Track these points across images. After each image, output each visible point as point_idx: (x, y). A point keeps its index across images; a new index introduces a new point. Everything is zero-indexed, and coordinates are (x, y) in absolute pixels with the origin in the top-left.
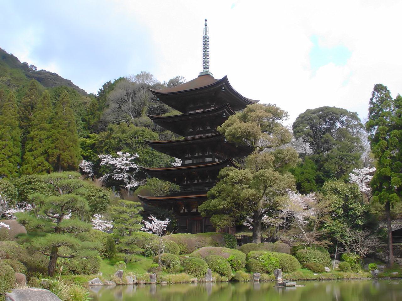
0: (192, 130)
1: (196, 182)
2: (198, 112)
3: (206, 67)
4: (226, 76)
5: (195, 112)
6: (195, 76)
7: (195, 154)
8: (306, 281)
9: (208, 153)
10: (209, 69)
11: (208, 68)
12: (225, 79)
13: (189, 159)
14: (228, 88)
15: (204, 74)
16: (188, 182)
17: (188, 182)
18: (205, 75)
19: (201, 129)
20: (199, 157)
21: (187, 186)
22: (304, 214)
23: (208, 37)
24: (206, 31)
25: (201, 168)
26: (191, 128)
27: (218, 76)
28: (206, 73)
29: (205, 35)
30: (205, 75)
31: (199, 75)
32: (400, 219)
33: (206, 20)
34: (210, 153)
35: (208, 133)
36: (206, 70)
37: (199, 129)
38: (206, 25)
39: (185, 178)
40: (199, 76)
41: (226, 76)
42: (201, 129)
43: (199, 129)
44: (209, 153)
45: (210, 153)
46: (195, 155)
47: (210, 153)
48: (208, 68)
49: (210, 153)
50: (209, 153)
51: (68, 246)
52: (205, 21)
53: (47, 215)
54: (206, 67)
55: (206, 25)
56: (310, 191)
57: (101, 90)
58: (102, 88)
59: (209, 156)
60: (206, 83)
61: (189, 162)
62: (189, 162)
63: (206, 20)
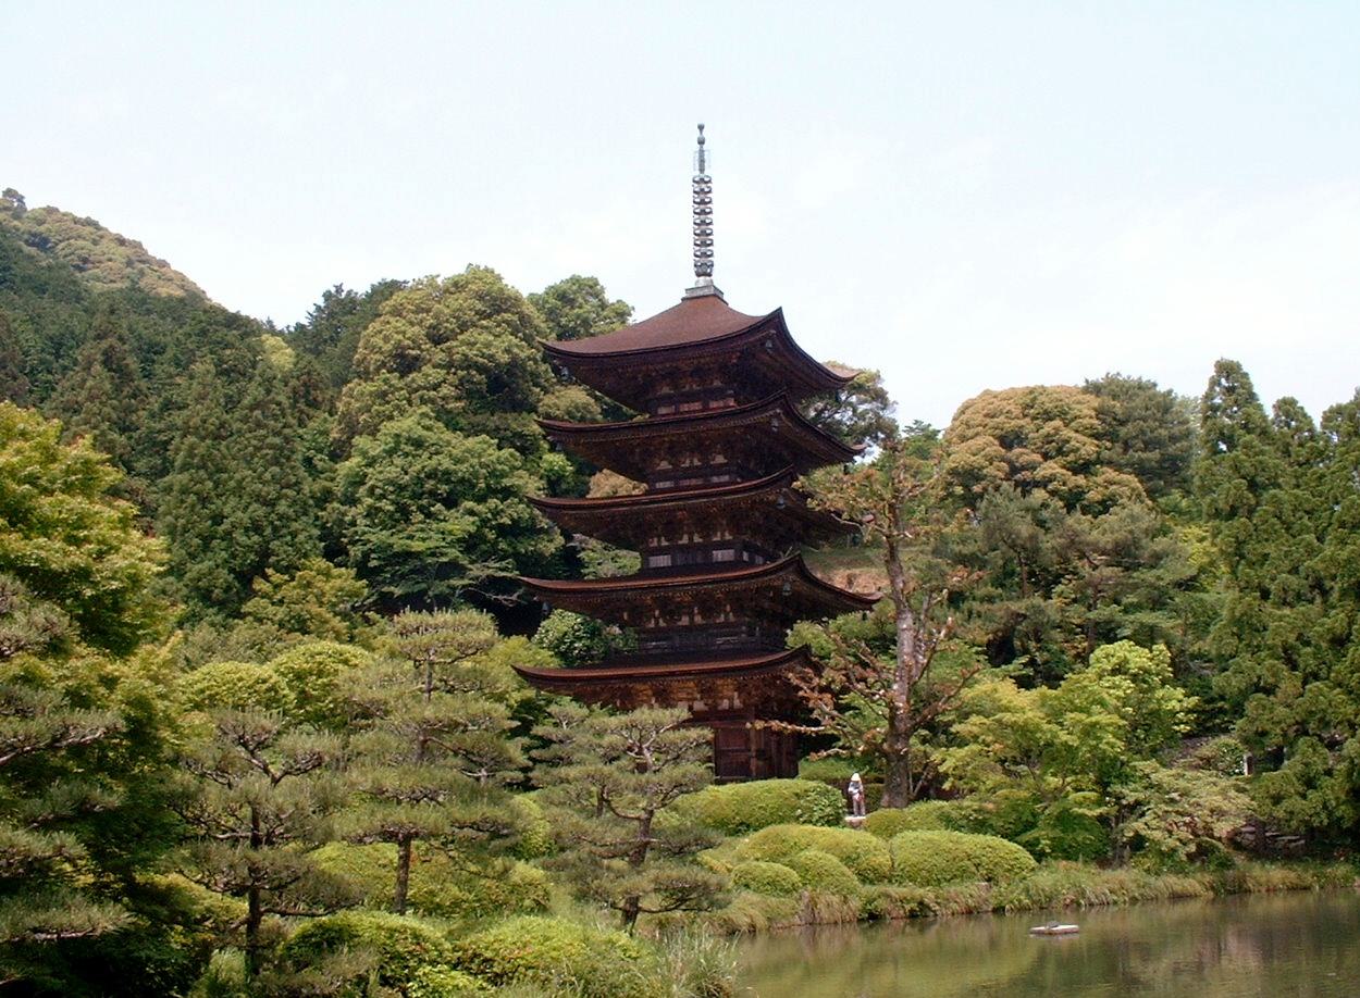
0: (670, 463)
1: (685, 621)
3: (704, 269)
4: (780, 309)
6: (672, 298)
11: (710, 275)
12: (776, 320)
13: (660, 551)
14: (785, 345)
15: (700, 293)
18: (705, 300)
19: (696, 462)
20: (691, 547)
21: (657, 634)
22: (125, 669)
24: (702, 161)
27: (748, 300)
29: (698, 173)
30: (705, 300)
31: (684, 295)
33: (701, 128)
34: (727, 534)
35: (718, 475)
37: (692, 462)
38: (701, 142)
40: (683, 299)
41: (780, 309)
42: (696, 462)
43: (692, 462)
44: (723, 535)
45: (728, 537)
47: (727, 534)
48: (710, 275)
49: (728, 537)
50: (723, 535)
54: (704, 269)
55: (701, 142)
56: (317, 334)
57: (318, 308)
58: (323, 299)
59: (723, 545)
60: (706, 328)
61: (663, 561)
62: (663, 561)
63: (701, 128)
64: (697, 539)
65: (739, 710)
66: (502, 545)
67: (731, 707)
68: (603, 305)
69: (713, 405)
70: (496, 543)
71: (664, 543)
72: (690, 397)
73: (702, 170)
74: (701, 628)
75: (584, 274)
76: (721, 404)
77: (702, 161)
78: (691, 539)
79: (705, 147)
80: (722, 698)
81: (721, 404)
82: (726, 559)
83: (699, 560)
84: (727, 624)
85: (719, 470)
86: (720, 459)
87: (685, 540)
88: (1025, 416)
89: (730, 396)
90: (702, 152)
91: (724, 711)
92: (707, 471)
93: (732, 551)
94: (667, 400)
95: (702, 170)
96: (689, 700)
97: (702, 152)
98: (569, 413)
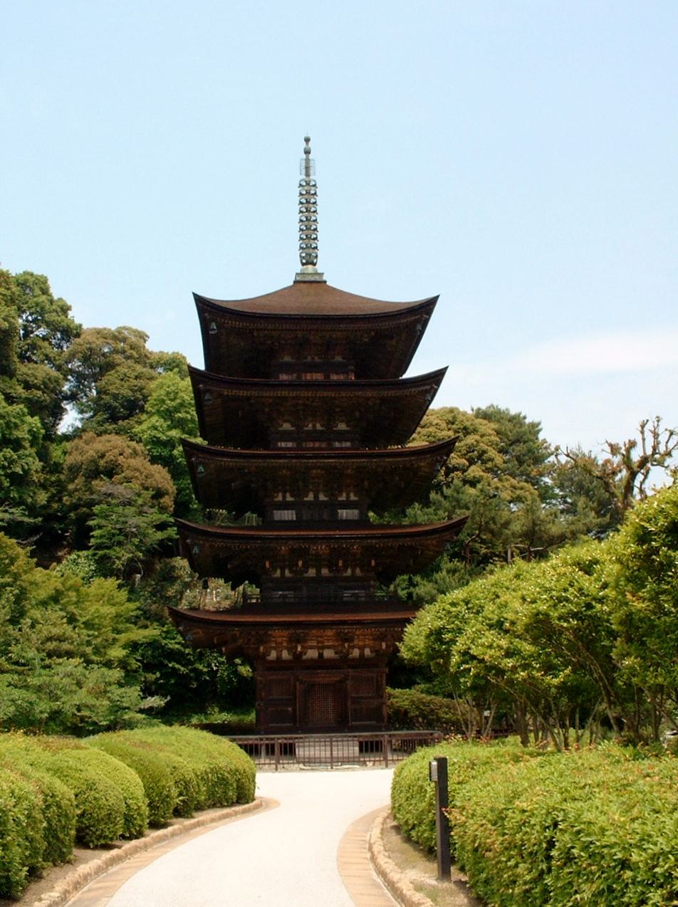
2: (308, 378)
5: (299, 377)
7: (307, 496)
8: (369, 855)
9: (344, 495)
10: (317, 267)
11: (314, 264)
13: (285, 506)
16: (287, 572)
17: (287, 572)
18: (310, 284)
19: (319, 427)
20: (316, 504)
23: (312, 183)
24: (307, 168)
25: (276, 539)
26: (342, 421)
28: (317, 278)
29: (304, 177)
30: (310, 284)
32: (586, 684)
33: (307, 140)
35: (340, 441)
36: (310, 268)
38: (307, 152)
39: (376, 564)
42: (319, 427)
45: (353, 497)
46: (305, 499)
50: (348, 496)
51: (56, 772)
52: (304, 143)
53: (308, 668)
55: (307, 152)
59: (347, 505)
62: (289, 515)
63: (307, 140)
64: (322, 497)
65: (285, 661)
66: (14, 494)
67: (362, 655)
68: (52, 302)
69: (334, 377)
70: (8, 491)
71: (289, 498)
72: (313, 368)
73: (308, 175)
74: (328, 580)
75: (37, 272)
76: (342, 377)
77: (307, 168)
78: (316, 497)
79: (311, 156)
80: (353, 647)
81: (342, 377)
82: (350, 517)
83: (325, 517)
84: (353, 578)
85: (341, 436)
86: (342, 426)
87: (310, 497)
88: (449, 429)
89: (351, 371)
90: (307, 160)
91: (354, 659)
92: (329, 435)
93: (356, 512)
94: (288, 368)
95: (308, 175)
96: (319, 648)
97: (307, 160)
98: (44, 383)
